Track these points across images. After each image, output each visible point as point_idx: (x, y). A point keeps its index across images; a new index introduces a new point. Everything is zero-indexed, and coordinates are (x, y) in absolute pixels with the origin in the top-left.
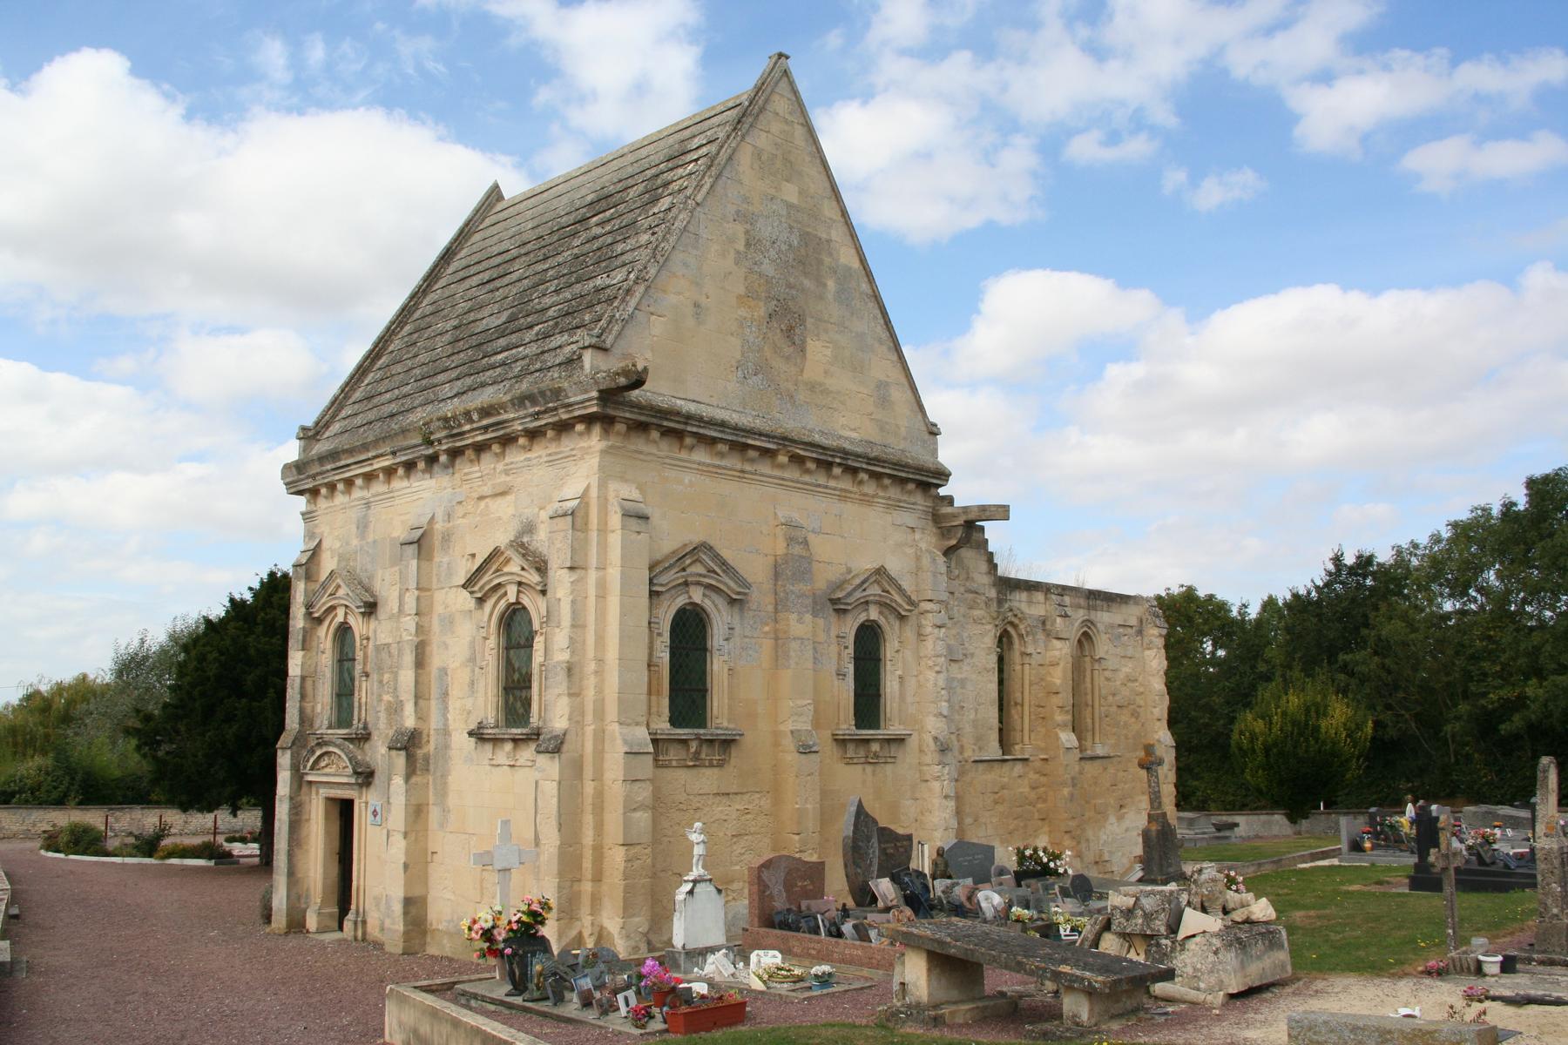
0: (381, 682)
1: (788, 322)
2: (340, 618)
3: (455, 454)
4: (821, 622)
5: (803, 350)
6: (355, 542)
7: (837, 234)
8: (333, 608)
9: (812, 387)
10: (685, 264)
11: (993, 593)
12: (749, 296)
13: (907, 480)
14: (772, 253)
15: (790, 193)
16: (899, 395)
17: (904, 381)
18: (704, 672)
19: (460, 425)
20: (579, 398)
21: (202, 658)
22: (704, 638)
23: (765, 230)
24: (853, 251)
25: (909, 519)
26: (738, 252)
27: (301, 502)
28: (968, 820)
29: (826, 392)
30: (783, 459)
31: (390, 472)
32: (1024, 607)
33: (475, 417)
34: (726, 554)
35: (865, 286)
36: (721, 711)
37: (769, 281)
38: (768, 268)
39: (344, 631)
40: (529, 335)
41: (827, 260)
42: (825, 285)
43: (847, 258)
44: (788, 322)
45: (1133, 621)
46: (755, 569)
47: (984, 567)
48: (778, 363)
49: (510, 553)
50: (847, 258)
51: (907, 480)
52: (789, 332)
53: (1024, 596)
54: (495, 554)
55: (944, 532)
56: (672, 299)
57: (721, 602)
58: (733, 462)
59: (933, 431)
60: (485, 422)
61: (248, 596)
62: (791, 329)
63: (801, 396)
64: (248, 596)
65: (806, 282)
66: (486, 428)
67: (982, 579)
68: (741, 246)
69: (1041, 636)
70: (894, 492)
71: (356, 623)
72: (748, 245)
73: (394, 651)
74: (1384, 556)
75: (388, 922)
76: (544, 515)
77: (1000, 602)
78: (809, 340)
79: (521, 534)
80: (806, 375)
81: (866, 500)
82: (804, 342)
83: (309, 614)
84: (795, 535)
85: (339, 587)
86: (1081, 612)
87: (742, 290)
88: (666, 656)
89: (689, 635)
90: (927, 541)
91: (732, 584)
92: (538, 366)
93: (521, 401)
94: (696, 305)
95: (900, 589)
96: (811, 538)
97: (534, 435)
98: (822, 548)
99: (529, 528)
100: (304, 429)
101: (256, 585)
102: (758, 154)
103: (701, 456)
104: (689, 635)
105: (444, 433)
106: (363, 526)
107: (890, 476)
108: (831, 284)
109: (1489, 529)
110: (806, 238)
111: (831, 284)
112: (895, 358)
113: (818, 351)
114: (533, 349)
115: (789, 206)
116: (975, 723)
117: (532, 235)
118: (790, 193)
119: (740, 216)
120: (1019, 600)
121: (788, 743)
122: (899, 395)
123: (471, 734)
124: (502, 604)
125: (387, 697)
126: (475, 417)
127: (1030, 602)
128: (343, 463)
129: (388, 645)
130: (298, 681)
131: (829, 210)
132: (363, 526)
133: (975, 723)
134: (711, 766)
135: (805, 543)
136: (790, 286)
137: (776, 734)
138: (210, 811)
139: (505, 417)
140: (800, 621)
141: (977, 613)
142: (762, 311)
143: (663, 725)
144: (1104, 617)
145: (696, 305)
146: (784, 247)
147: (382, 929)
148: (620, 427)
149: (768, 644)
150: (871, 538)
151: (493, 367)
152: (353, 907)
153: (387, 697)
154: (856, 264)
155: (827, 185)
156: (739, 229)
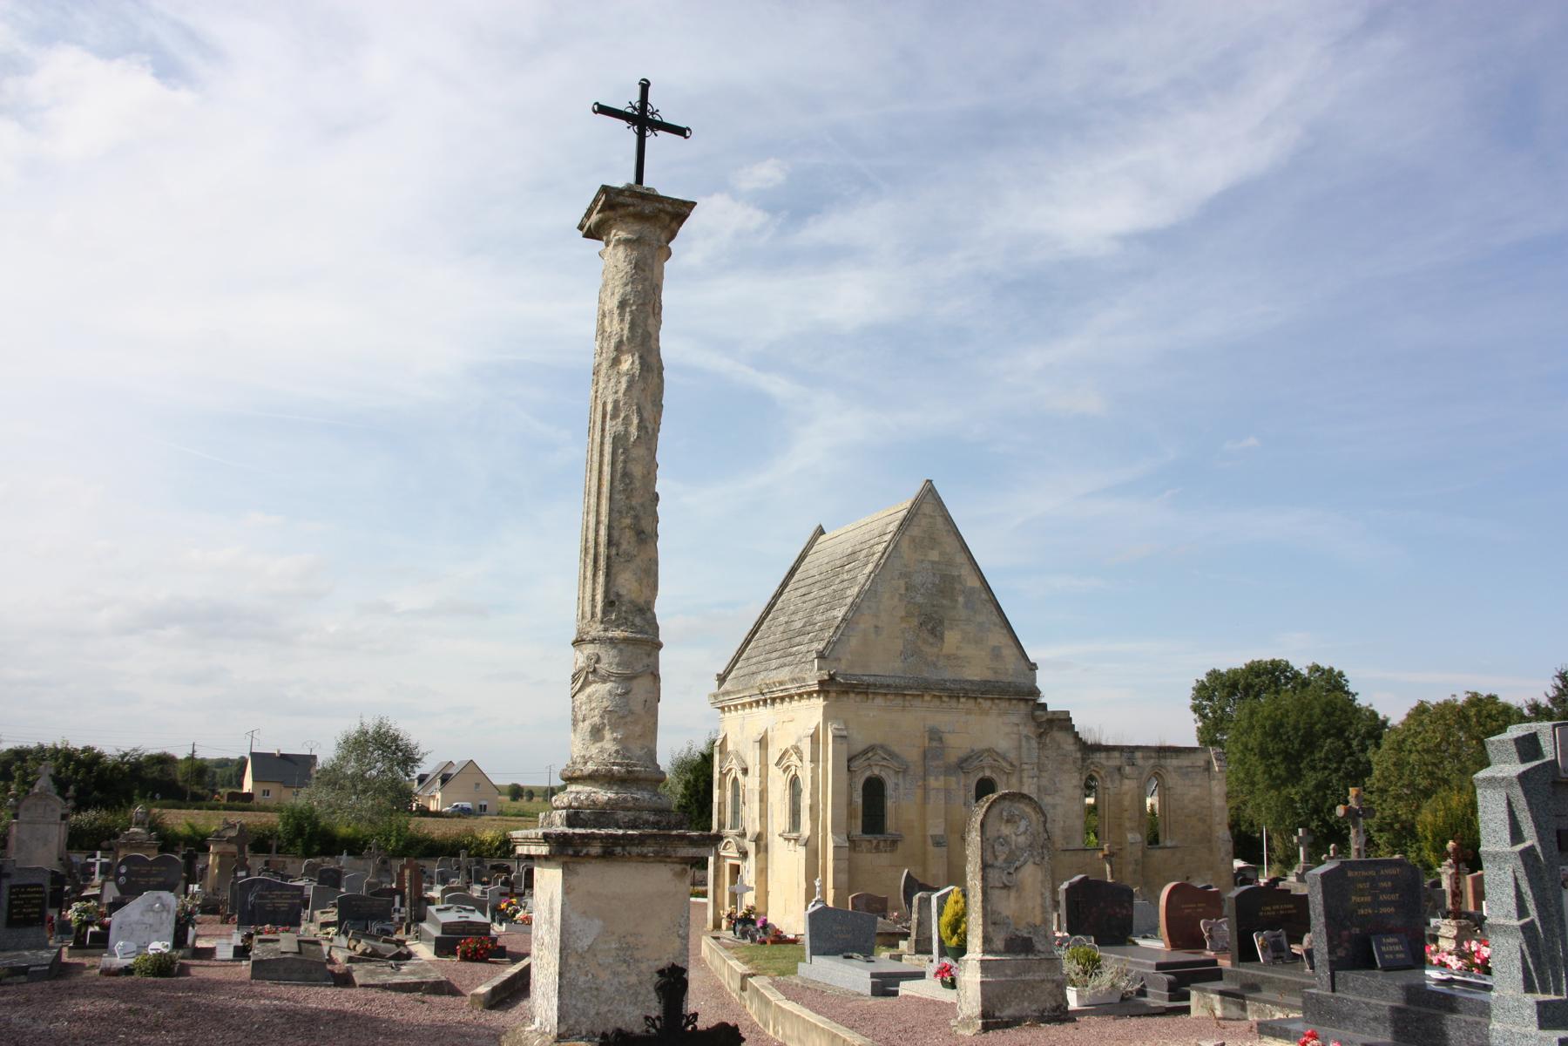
1: (932, 624)
3: (773, 700)
4: (954, 779)
5: (942, 639)
7: (966, 571)
9: (948, 657)
11: (1079, 755)
12: (909, 615)
15: (934, 555)
17: (1011, 642)
23: (917, 580)
25: (1015, 719)
29: (957, 658)
31: (751, 704)
32: (1104, 762)
36: (890, 823)
37: (920, 606)
38: (920, 599)
39: (735, 779)
41: (958, 586)
46: (912, 754)
47: (1071, 740)
48: (926, 649)
50: (973, 582)
52: (933, 632)
53: (1103, 755)
54: (786, 751)
55: (1039, 725)
56: (862, 626)
58: (899, 701)
63: (940, 664)
67: (1069, 746)
69: (1117, 776)
70: (1004, 704)
71: (740, 776)
77: (1084, 760)
80: (945, 651)
81: (986, 713)
84: (935, 735)
88: (860, 801)
89: (874, 792)
90: (1028, 730)
93: (793, 680)
97: (801, 696)
98: (951, 740)
102: (913, 539)
103: (879, 701)
104: (874, 792)
106: (742, 728)
108: (961, 599)
109: (1454, 707)
110: (944, 577)
115: (933, 563)
116: (1063, 829)
117: (828, 568)
118: (934, 555)
119: (903, 575)
120: (1100, 757)
121: (930, 841)
127: (1108, 758)
131: (960, 558)
132: (742, 728)
133: (1063, 829)
135: (941, 739)
137: (924, 836)
140: (937, 779)
141: (1066, 767)
142: (915, 622)
143: (857, 831)
144: (1173, 762)
149: (919, 792)
150: (992, 731)
154: (977, 584)
156: (902, 583)
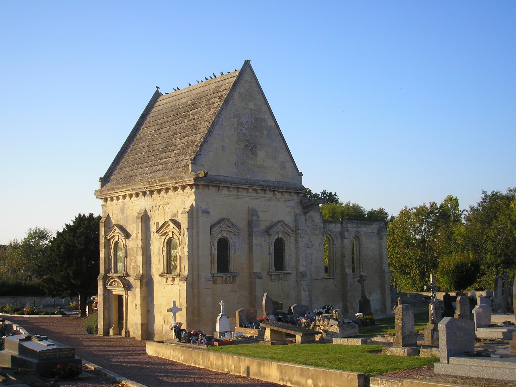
0: (131, 259)
1: (250, 147)
2: (116, 239)
4: (263, 239)
6: (120, 216)
8: (114, 236)
10: (219, 134)
11: (322, 225)
13: (291, 193)
14: (246, 126)
15: (251, 106)
16: (289, 165)
18: (227, 256)
19: (153, 184)
20: (188, 179)
21: (59, 247)
22: (227, 246)
24: (273, 121)
26: (235, 128)
27: (101, 202)
28: (314, 298)
30: (250, 190)
33: (158, 182)
34: (233, 221)
35: (277, 132)
38: (245, 131)
40: (173, 154)
42: (263, 133)
43: (271, 123)
44: (250, 147)
45: (375, 231)
49: (170, 223)
51: (291, 193)
54: (166, 222)
57: (232, 235)
59: (300, 174)
60: (161, 184)
61: (72, 224)
62: (252, 149)
64: (72, 224)
65: (257, 133)
66: (161, 185)
68: (236, 126)
70: (287, 196)
72: (238, 125)
73: (135, 250)
74: (504, 192)
75: (136, 331)
76: (180, 212)
77: (324, 228)
78: (258, 152)
79: (173, 217)
82: (256, 152)
83: (106, 238)
85: (116, 230)
86: (355, 229)
87: (236, 139)
91: (235, 230)
92: (176, 166)
94: (222, 146)
95: (289, 227)
96: (259, 213)
99: (176, 215)
100: (101, 178)
101: (74, 219)
103: (225, 191)
104: (223, 246)
105: (148, 186)
107: (285, 192)
111: (265, 132)
112: (287, 153)
113: (261, 154)
114: (173, 160)
115: (251, 110)
118: (251, 106)
122: (289, 165)
123: (159, 275)
124: (168, 237)
125: (133, 264)
126: (158, 182)
128: (116, 191)
129: (133, 248)
130: (104, 258)
134: (230, 283)
136: (252, 136)
138: (53, 298)
139: (167, 183)
141: (317, 232)
143: (215, 271)
145: (222, 146)
146: (250, 123)
147: (134, 333)
148: (201, 187)
151: (161, 164)
152: (124, 327)
153: (133, 264)
154: (274, 124)
155: (264, 100)
